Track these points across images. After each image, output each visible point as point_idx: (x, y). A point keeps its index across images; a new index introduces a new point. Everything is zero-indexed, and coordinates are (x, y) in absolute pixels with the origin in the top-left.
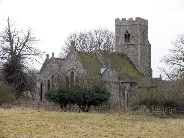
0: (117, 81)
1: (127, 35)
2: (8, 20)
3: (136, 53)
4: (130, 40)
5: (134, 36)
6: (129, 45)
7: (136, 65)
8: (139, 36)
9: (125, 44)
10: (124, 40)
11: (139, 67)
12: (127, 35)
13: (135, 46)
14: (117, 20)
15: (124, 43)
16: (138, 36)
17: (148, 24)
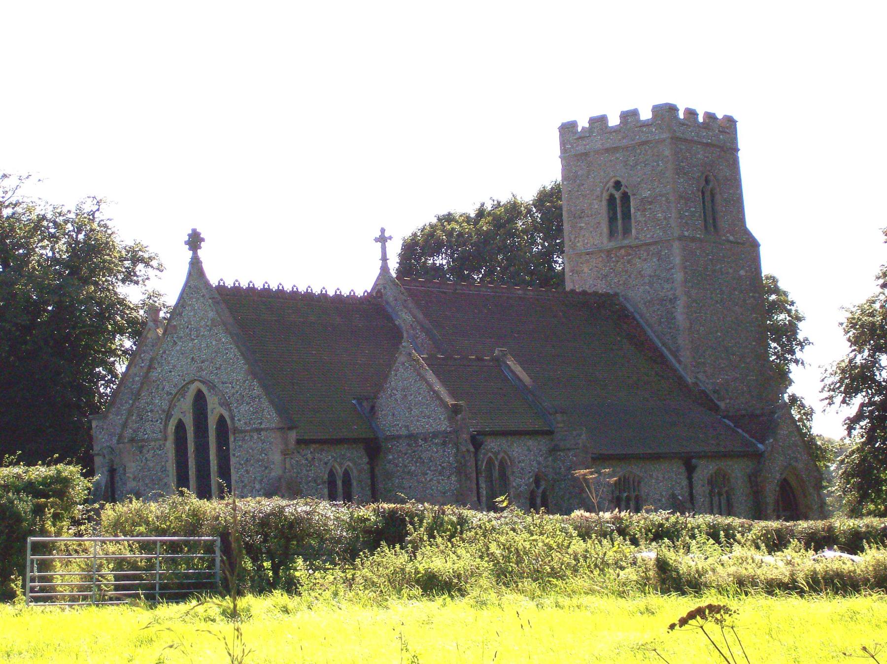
0: (444, 426)
1: (618, 201)
3: (666, 286)
4: (633, 224)
5: (650, 203)
8: (672, 199)
9: (612, 244)
10: (605, 229)
11: (686, 356)
12: (618, 201)
13: (659, 253)
14: (567, 130)
15: (605, 240)
17: (736, 138)
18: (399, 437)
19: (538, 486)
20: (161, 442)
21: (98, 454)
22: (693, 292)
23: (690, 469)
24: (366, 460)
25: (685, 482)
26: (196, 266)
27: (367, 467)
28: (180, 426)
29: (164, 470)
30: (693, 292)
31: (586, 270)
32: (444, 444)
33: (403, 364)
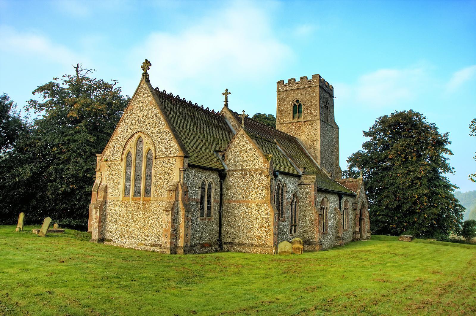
2: (77, 68)
3: (314, 136)
5: (310, 107)
6: (301, 122)
7: (313, 157)
9: (294, 121)
14: (280, 83)
15: (292, 119)
16: (316, 107)
18: (236, 170)
19: (294, 199)
20: (119, 162)
21: (98, 171)
22: (322, 139)
23: (340, 198)
24: (219, 180)
25: (338, 204)
26: (146, 77)
27: (219, 183)
28: (129, 154)
29: (119, 176)
30: (322, 139)
31: (283, 129)
32: (261, 174)
33: (241, 135)
